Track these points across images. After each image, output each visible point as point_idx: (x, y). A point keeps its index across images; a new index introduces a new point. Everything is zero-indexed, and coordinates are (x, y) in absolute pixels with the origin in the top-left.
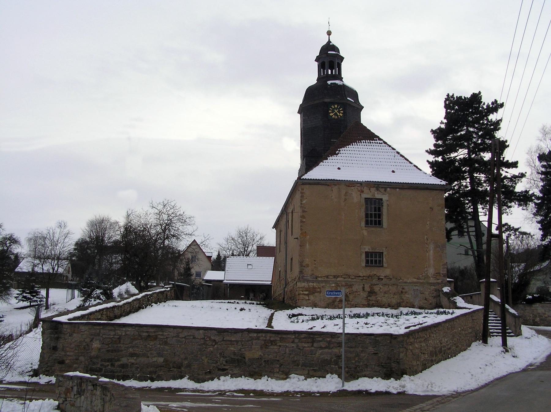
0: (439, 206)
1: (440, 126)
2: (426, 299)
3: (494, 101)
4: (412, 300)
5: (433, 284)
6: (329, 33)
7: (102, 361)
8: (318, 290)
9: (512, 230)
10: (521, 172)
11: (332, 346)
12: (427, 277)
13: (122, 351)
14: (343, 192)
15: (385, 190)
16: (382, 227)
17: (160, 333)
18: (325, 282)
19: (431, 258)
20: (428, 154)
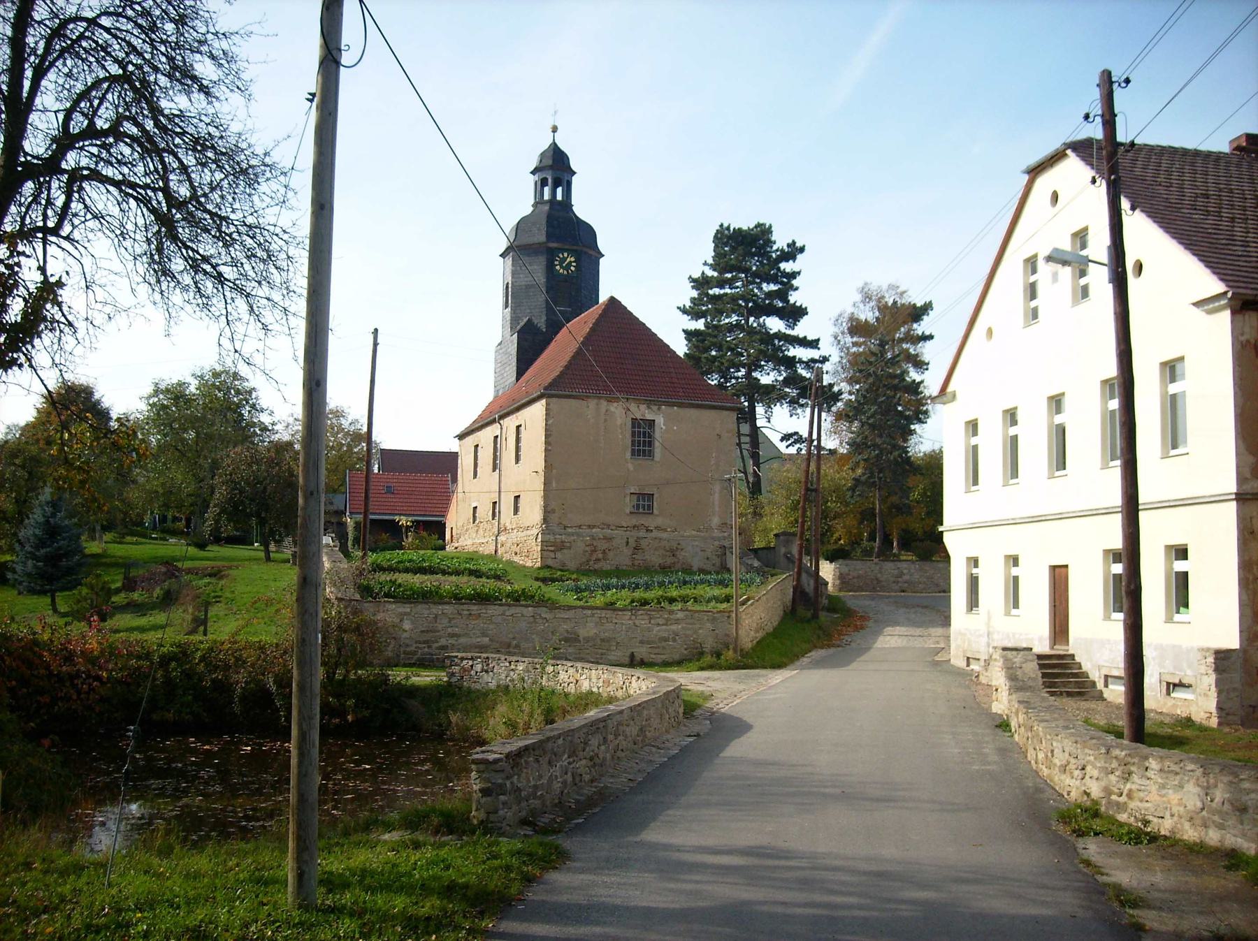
0: (728, 432)
1: (703, 273)
2: (708, 558)
3: (790, 242)
4: (689, 560)
5: (719, 539)
6: (555, 129)
7: (416, 643)
8: (568, 544)
9: (803, 442)
10: (823, 354)
11: (669, 623)
12: (710, 529)
13: (439, 631)
14: (603, 410)
15: (659, 409)
16: (653, 460)
17: (484, 611)
18: (578, 535)
19: (717, 503)
20: (681, 313)
